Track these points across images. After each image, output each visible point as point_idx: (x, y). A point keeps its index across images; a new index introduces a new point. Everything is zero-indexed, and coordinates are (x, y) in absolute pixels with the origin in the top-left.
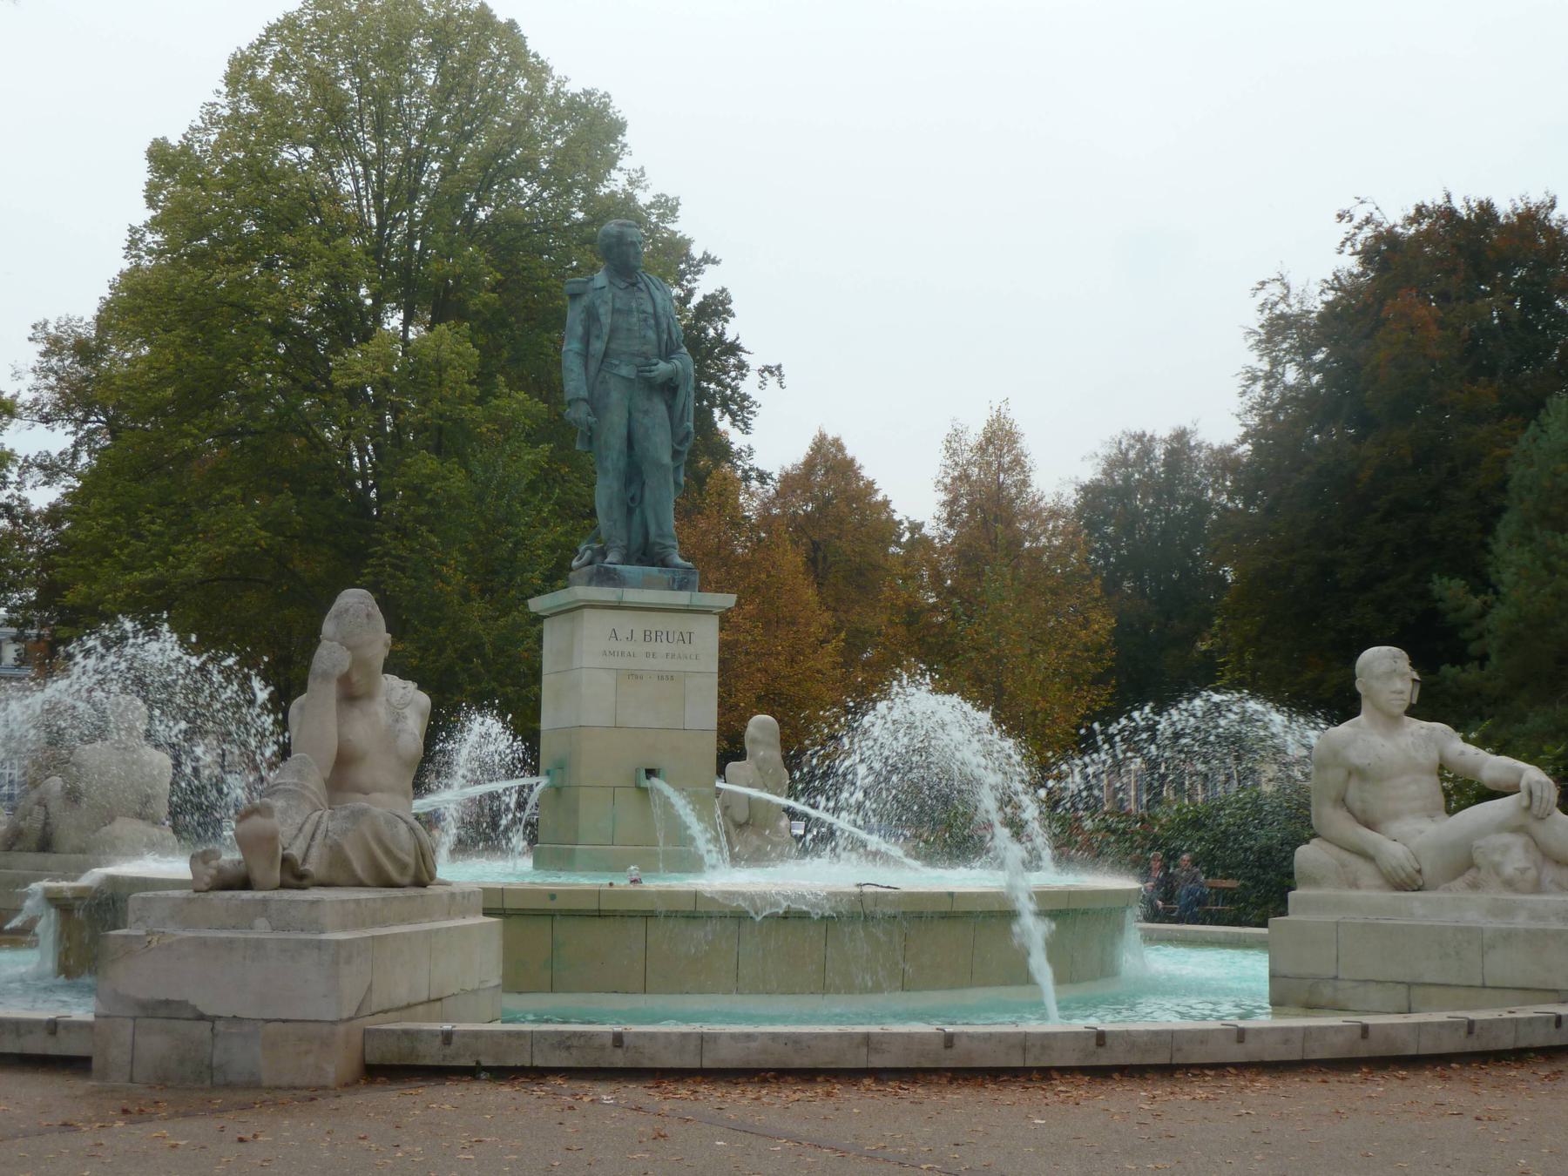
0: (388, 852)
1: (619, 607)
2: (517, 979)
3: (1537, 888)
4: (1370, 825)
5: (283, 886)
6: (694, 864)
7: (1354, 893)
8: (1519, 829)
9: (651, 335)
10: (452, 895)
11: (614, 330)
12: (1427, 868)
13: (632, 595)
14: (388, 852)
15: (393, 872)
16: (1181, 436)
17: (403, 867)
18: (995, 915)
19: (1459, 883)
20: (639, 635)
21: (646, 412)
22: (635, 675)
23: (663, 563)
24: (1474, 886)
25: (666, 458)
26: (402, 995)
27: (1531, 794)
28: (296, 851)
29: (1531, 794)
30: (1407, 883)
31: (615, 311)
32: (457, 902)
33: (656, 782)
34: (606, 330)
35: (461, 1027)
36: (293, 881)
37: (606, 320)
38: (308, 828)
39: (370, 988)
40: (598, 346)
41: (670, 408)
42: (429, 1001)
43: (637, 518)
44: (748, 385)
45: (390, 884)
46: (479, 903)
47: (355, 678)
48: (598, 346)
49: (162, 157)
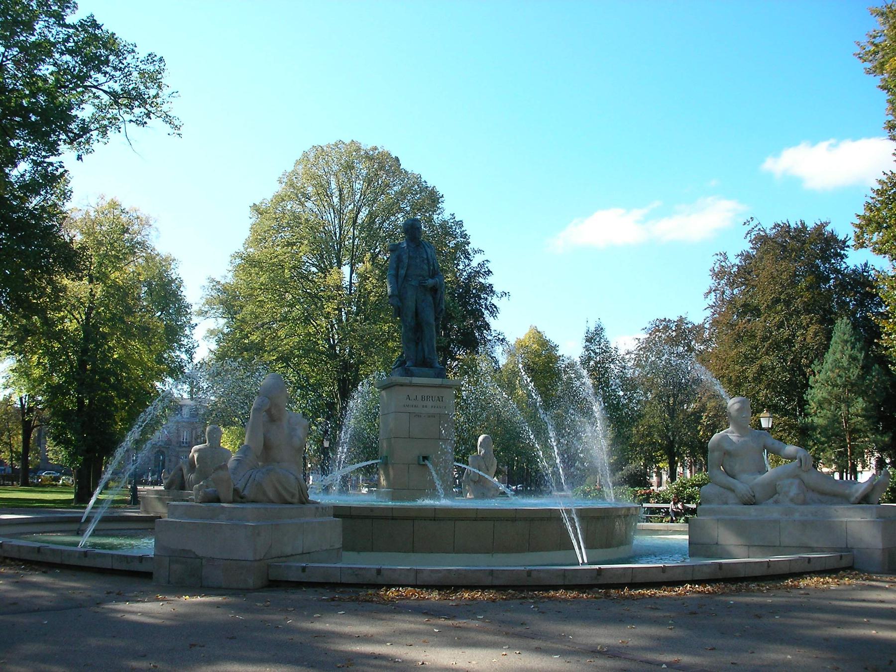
0: (285, 489)
1: (411, 385)
2: (350, 545)
3: (805, 503)
4: (733, 477)
5: (234, 502)
6: (439, 498)
7: (725, 507)
8: (797, 476)
9: (426, 267)
10: (317, 508)
11: (409, 266)
12: (757, 495)
13: (416, 380)
14: (285, 489)
15: (289, 498)
16: (681, 320)
17: (293, 496)
18: (552, 517)
19: (771, 501)
20: (419, 398)
21: (423, 301)
22: (418, 416)
23: (431, 366)
24: (776, 502)
25: (432, 321)
26: (288, 550)
27: (801, 460)
28: (240, 486)
29: (801, 460)
30: (751, 501)
31: (410, 257)
32: (322, 510)
33: (426, 462)
34: (406, 265)
35: (310, 565)
36: (239, 499)
37: (405, 260)
38: (247, 476)
39: (271, 547)
40: (402, 272)
41: (434, 298)
42: (303, 553)
43: (420, 347)
44: (495, 301)
45: (286, 502)
46: (332, 512)
47: (273, 411)
48: (402, 272)
49: (257, 209)
